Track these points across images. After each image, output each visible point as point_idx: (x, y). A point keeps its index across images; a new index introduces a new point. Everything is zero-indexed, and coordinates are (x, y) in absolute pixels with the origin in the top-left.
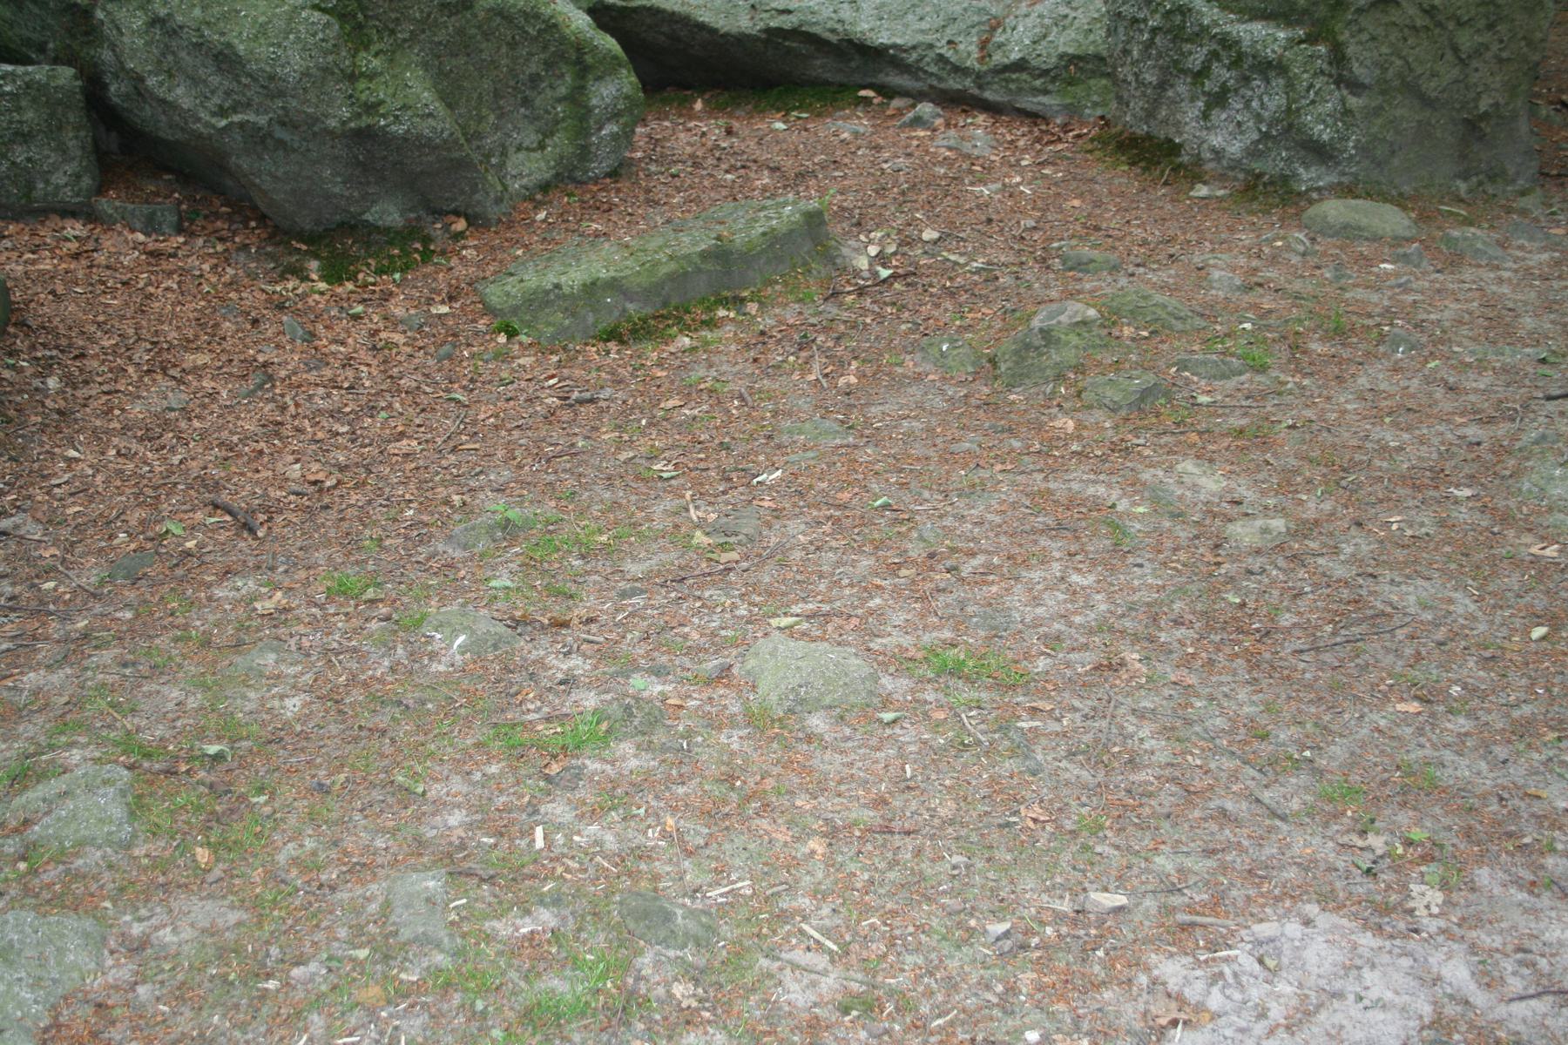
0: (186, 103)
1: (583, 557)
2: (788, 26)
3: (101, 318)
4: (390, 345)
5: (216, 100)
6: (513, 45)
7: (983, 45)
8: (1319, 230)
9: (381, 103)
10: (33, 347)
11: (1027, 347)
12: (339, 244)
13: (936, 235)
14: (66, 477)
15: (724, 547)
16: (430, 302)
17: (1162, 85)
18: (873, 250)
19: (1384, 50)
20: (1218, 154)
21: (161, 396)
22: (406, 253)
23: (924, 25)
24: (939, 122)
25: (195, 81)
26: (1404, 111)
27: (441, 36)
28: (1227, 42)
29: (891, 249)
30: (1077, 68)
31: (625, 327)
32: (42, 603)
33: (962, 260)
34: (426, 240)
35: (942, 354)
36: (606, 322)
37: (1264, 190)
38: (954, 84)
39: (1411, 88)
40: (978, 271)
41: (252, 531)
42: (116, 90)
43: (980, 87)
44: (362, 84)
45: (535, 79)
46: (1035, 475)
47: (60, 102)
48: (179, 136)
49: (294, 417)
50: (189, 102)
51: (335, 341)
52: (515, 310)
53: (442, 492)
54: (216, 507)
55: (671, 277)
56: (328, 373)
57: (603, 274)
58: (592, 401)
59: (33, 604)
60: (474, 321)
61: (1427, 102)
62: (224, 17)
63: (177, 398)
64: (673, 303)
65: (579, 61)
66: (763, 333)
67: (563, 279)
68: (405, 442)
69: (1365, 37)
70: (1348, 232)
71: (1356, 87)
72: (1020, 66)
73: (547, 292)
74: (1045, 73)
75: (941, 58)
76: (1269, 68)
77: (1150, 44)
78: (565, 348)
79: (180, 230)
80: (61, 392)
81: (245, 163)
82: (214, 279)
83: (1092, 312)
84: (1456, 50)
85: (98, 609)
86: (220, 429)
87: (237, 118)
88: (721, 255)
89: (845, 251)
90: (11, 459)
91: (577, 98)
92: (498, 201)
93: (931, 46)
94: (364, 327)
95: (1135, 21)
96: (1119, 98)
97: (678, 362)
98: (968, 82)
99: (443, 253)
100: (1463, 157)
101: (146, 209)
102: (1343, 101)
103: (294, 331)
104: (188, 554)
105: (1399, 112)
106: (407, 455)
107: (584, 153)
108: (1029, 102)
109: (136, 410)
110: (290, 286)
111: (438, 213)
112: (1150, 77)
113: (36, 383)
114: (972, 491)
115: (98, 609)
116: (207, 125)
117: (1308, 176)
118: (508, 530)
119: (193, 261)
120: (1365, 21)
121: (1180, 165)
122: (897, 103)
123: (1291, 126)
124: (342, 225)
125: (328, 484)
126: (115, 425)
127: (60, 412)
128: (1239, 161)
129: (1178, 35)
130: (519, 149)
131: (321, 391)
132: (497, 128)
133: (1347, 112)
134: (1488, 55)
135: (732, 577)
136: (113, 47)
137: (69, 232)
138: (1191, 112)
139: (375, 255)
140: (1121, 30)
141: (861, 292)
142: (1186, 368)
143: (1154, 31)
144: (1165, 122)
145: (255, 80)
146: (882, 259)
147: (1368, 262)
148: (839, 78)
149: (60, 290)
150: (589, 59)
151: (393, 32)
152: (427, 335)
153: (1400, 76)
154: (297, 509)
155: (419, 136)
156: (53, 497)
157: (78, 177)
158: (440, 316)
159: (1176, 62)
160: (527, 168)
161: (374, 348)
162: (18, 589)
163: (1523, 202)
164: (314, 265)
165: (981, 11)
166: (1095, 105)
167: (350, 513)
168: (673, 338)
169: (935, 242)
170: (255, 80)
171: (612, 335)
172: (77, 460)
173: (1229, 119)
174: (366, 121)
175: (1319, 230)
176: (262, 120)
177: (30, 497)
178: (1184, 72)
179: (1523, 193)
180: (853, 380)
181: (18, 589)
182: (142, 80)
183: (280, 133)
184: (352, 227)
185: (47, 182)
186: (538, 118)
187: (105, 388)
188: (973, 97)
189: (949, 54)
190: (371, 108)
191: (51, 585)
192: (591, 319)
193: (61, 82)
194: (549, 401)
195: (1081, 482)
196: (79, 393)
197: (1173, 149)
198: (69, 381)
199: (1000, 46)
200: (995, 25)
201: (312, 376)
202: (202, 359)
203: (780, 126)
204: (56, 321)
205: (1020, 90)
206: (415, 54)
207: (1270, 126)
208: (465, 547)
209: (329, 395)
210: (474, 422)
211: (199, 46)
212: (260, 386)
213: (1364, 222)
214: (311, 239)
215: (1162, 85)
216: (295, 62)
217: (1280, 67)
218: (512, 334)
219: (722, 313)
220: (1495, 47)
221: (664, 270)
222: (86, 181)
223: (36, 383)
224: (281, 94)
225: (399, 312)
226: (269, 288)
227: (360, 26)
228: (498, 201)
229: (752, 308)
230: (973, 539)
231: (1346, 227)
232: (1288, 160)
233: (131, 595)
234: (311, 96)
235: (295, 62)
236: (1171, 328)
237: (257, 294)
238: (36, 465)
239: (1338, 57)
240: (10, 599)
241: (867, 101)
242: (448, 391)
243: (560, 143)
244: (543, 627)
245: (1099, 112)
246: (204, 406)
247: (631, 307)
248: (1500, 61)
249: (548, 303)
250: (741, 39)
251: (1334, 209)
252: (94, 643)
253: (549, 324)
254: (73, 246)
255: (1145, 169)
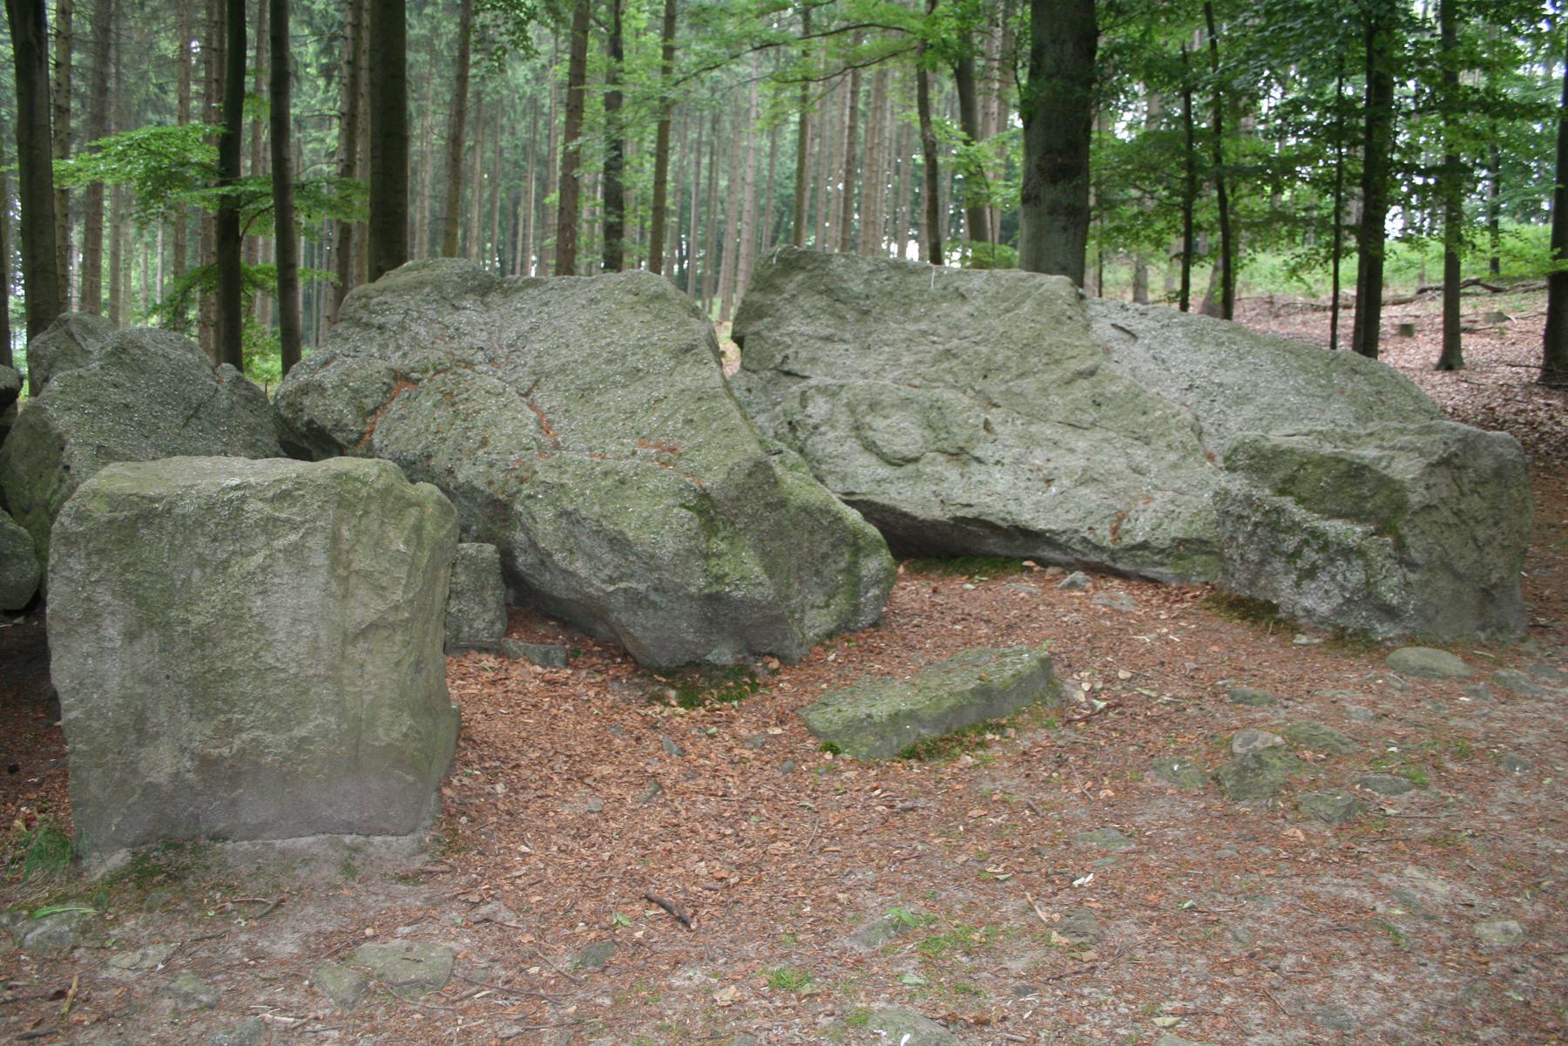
0: (583, 573)
1: (967, 954)
2: (970, 516)
3: (524, 734)
4: (743, 760)
5: (607, 572)
6: (811, 533)
7: (1114, 531)
8: (1405, 670)
9: (726, 575)
10: (481, 758)
11: (1245, 769)
12: (689, 678)
13: (1129, 675)
14: (524, 869)
15: (1082, 948)
16: (766, 725)
17: (1262, 563)
18: (1086, 686)
19: (1430, 540)
20: (1309, 612)
21: (575, 804)
22: (738, 685)
23: (1070, 516)
24: (1089, 585)
25: (591, 557)
26: (1443, 582)
27: (765, 526)
28: (1314, 533)
29: (1099, 686)
30: (1184, 548)
31: (921, 747)
32: (533, 988)
33: (1153, 694)
34: (752, 675)
35: (1174, 773)
36: (907, 743)
37: (1346, 639)
38: (1094, 557)
39: (1447, 567)
40: (1168, 703)
41: (686, 923)
42: (522, 561)
43: (1114, 560)
44: (713, 561)
45: (825, 556)
46: (1295, 879)
47: (484, 570)
48: (573, 596)
49: (687, 819)
50: (586, 573)
51: (700, 756)
52: (837, 734)
53: (827, 891)
54: (651, 900)
55: (952, 709)
56: (701, 782)
57: (903, 707)
58: (913, 809)
59: (526, 987)
60: (803, 741)
61: (1458, 576)
62: (616, 512)
63: (594, 803)
64: (955, 728)
65: (855, 544)
66: (1025, 753)
67: (874, 711)
68: (779, 844)
69: (1417, 531)
70: (1425, 673)
71: (1412, 566)
72: (1144, 546)
73: (862, 721)
74: (1162, 551)
75: (1084, 539)
76: (1348, 552)
77: (1254, 533)
78: (878, 764)
79: (567, 664)
80: (507, 796)
81: (624, 617)
82: (599, 703)
83: (1278, 740)
84: (1475, 540)
85: (581, 995)
86: (632, 829)
87: (623, 585)
88: (985, 692)
89: (1067, 687)
90: (480, 853)
91: (852, 569)
92: (801, 645)
93: (1076, 531)
94: (724, 743)
95: (1241, 517)
96: (1225, 571)
97: (967, 777)
98: (1105, 557)
99: (766, 685)
100: (1482, 615)
101: (543, 648)
102: (1404, 576)
103: (670, 748)
104: (638, 943)
105: (1440, 584)
106: (784, 855)
107: (856, 610)
108: (1150, 572)
109: (566, 812)
110: (658, 709)
111: (758, 655)
112: (1253, 556)
113: (488, 788)
114: (1253, 894)
115: (581, 995)
116: (598, 589)
117: (1383, 630)
118: (901, 929)
119: (580, 689)
120: (1418, 520)
121: (1280, 620)
122: (1051, 570)
123: (1370, 594)
124: (689, 664)
125: (732, 881)
126: (551, 824)
127: (509, 813)
128: (1327, 618)
129: (1274, 527)
130: (812, 607)
131: (701, 798)
132: (799, 592)
133: (1408, 584)
134: (1495, 544)
135: (1098, 974)
136: (526, 531)
137: (485, 664)
138: (1286, 583)
139: (717, 686)
140: (1229, 524)
141: (1087, 720)
142: (1367, 785)
143: (1256, 524)
144: (1264, 588)
145: (639, 557)
146: (1093, 693)
147: (1450, 696)
148: (1005, 552)
149: (490, 711)
150: (861, 542)
151: (733, 524)
152: (769, 752)
153: (1440, 558)
154: (716, 903)
155: (753, 599)
156: (517, 886)
157: (493, 623)
158: (775, 736)
159: (1273, 547)
160: (818, 621)
161: (732, 762)
162: (510, 973)
163: (1523, 648)
164: (672, 693)
165: (1109, 507)
166: (1199, 574)
167: (759, 908)
168: (957, 758)
169: (1129, 680)
170: (639, 557)
171: (912, 754)
172: (529, 855)
173: (1318, 588)
174: (716, 588)
175: (1405, 670)
176: (642, 587)
177: (498, 887)
178: (1281, 554)
179: (1523, 640)
180: (1111, 793)
181: (510, 973)
182: (550, 555)
183: (654, 597)
184: (696, 665)
185: (471, 627)
186: (825, 584)
187: (539, 793)
188: (1108, 567)
189: (1090, 537)
190: (719, 579)
191: (534, 970)
192: (895, 742)
193: (486, 555)
194: (880, 808)
195: (1329, 885)
196: (521, 797)
197: (1274, 609)
198: (510, 785)
199: (1127, 532)
200: (1121, 517)
201: (690, 785)
202: (607, 770)
203: (969, 586)
204: (492, 735)
205: (1144, 563)
206: (748, 540)
207: (1353, 593)
208: (869, 944)
209: (708, 801)
210: (828, 827)
211: (598, 532)
212: (654, 793)
213: (1435, 665)
214: (668, 673)
215: (1262, 563)
216: (669, 546)
217: (1361, 553)
218: (836, 752)
219: (989, 736)
220: (1499, 538)
221: (947, 704)
222: (498, 626)
223: (488, 788)
224: (658, 568)
225: (743, 732)
226: (642, 712)
227: (712, 519)
228: (801, 645)
229: (1011, 732)
230: (1277, 939)
231: (1423, 668)
232: (1367, 618)
233: (605, 983)
234: (679, 570)
235: (669, 546)
236: (1339, 751)
237: (634, 716)
238: (498, 859)
239: (1400, 545)
240: (507, 982)
241: (1029, 569)
242: (796, 798)
243: (840, 602)
244: (968, 1026)
245: (1203, 579)
246: (616, 810)
247: (923, 731)
248: (1504, 547)
249: (861, 729)
250: (935, 525)
251: (1412, 655)
252: (590, 1030)
253: (863, 745)
254: (491, 674)
255: (1254, 622)
